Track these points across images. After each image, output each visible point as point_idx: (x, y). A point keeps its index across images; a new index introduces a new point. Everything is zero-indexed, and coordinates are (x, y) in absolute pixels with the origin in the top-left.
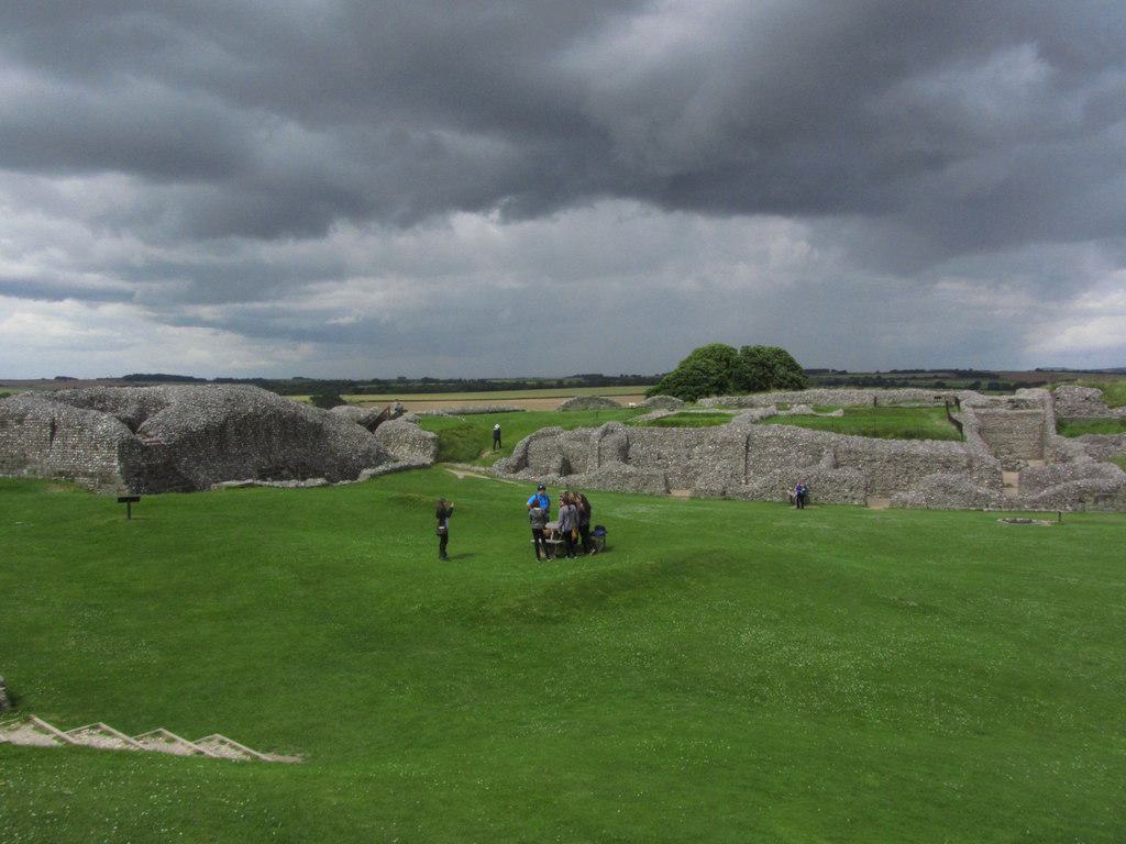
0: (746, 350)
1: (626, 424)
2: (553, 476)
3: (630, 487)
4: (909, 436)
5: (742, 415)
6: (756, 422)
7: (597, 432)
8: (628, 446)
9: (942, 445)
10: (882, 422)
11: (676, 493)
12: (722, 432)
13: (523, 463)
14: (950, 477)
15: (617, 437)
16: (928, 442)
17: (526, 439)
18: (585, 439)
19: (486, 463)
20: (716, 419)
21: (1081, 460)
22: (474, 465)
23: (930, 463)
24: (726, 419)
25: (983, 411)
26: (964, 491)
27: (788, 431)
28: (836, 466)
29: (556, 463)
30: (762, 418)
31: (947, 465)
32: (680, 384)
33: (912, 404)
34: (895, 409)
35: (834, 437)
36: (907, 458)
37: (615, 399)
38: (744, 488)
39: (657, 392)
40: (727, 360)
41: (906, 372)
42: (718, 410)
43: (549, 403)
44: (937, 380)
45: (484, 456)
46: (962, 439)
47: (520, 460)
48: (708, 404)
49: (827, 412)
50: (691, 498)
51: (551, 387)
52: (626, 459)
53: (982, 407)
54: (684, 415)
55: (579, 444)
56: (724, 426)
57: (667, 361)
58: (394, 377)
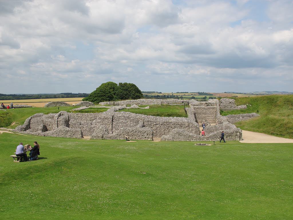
0: (121, 84)
1: (68, 112)
2: (40, 132)
3: (68, 136)
4: (169, 115)
5: (109, 109)
6: (116, 111)
7: (56, 115)
8: (69, 120)
9: (180, 118)
10: (160, 111)
11: (85, 137)
12: (103, 115)
13: (28, 127)
14: (181, 130)
15: (64, 116)
16: (175, 117)
17: (30, 118)
18: (53, 118)
19: (12, 128)
20: (102, 110)
21: (225, 123)
22: (8, 128)
23: (176, 125)
24: (105, 109)
25: (197, 107)
26: (185, 134)
27: (127, 114)
28: (144, 126)
29: (41, 127)
30: (119, 109)
31: (181, 126)
32: (95, 97)
33: (174, 104)
34: (168, 106)
35: (143, 116)
36: (168, 123)
37: (67, 103)
38: (110, 135)
39: (87, 100)
40: (114, 88)
41: (182, 93)
42: (105, 107)
43: (42, 104)
44: (192, 96)
45: (12, 125)
46: (186, 116)
47: (27, 126)
48: (102, 104)
49: (144, 107)
50: (91, 139)
51: (152, 97)
52: (68, 125)
53: (196, 105)
54: (92, 108)
55: (50, 120)
56: (104, 112)
57: (90, 90)
58: (78, 93)
